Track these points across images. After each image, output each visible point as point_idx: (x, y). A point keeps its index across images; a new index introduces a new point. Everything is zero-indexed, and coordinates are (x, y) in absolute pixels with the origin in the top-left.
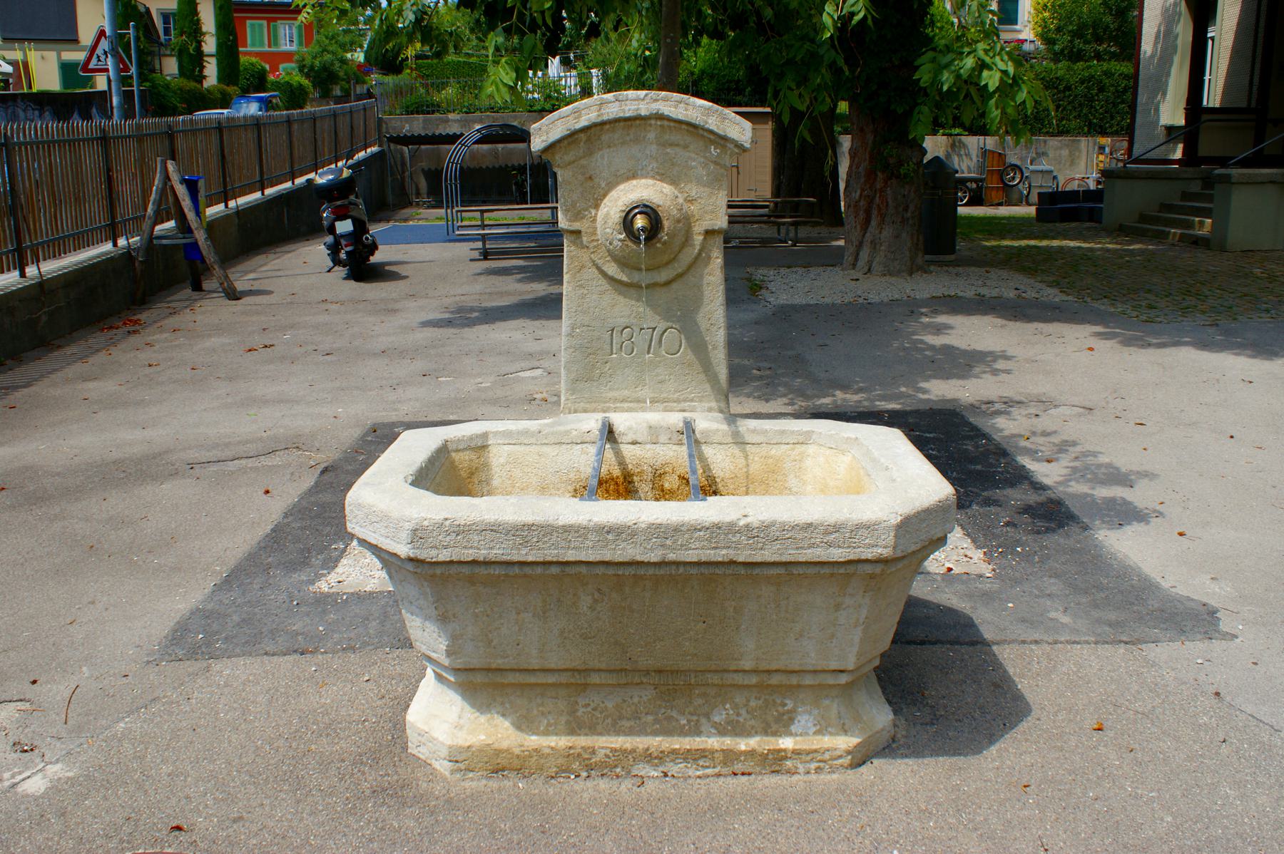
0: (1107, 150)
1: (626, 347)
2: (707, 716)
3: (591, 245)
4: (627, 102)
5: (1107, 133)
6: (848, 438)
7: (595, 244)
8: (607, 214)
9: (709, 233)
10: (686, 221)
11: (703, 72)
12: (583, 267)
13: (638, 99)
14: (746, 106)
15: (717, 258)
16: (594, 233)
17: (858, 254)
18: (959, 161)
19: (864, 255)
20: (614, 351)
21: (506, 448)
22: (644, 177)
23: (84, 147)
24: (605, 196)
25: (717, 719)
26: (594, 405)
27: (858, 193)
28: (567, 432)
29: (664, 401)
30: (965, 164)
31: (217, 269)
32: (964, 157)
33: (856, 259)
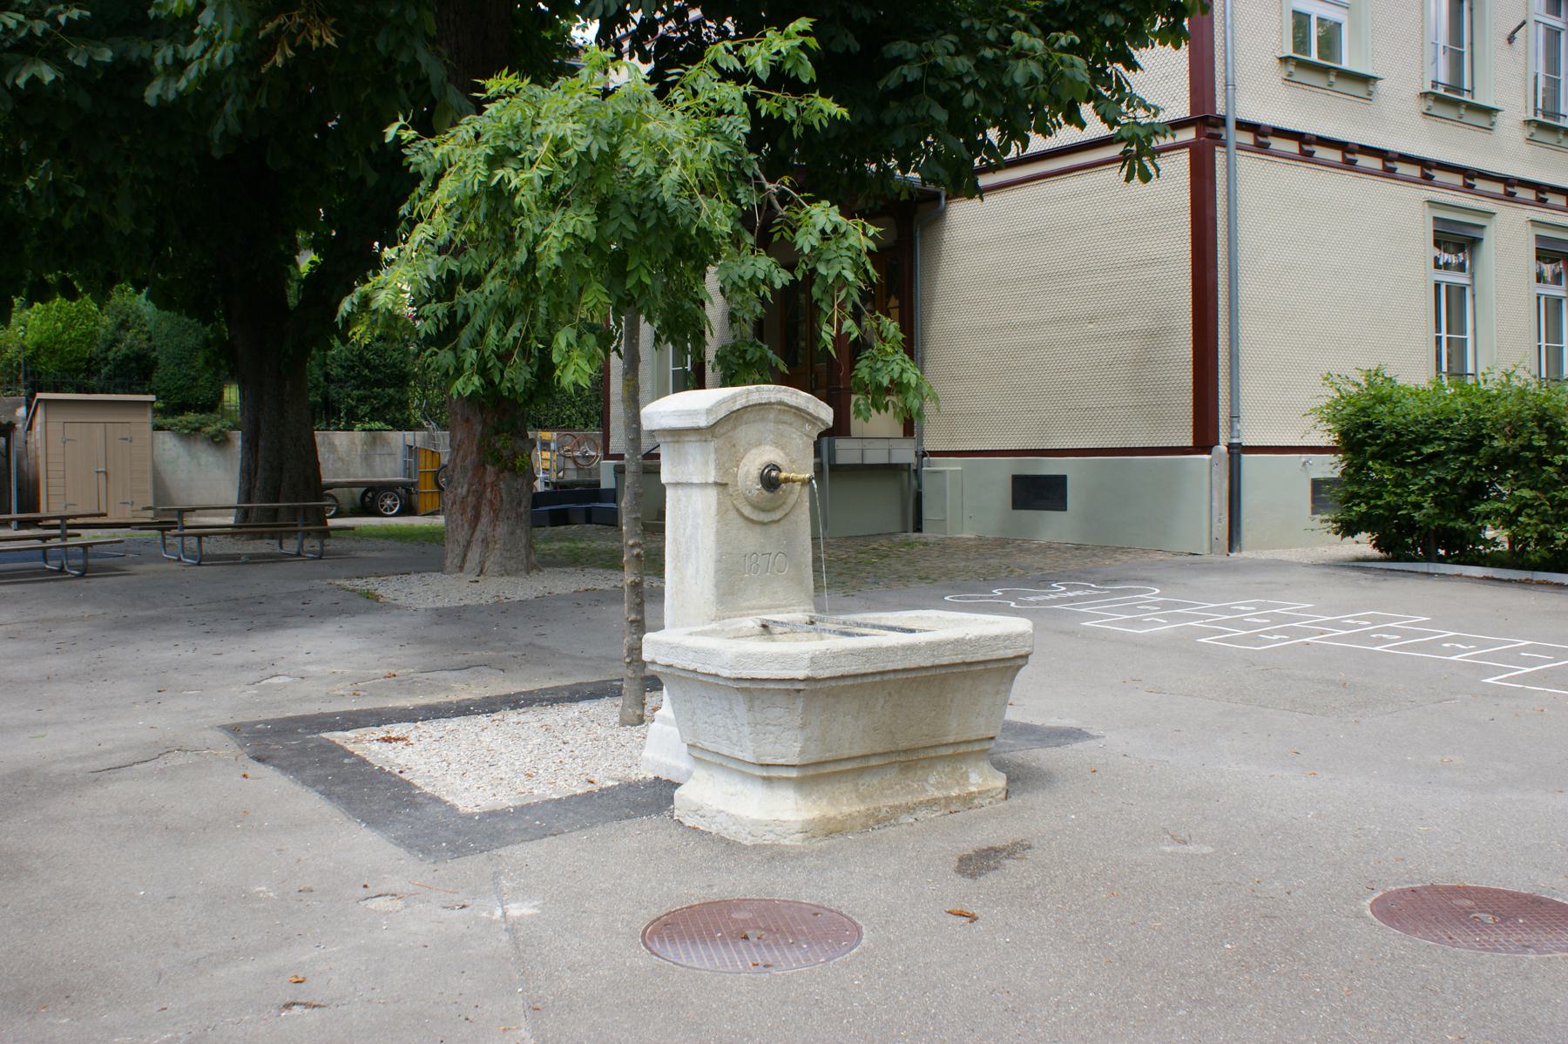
0: (553, 446)
2: (926, 781)
5: (546, 427)
11: (39, 346)
12: (727, 510)
13: (769, 390)
14: (102, 392)
16: (736, 485)
17: (465, 556)
19: (474, 555)
25: (931, 782)
26: (735, 613)
27: (466, 487)
28: (739, 630)
29: (779, 606)
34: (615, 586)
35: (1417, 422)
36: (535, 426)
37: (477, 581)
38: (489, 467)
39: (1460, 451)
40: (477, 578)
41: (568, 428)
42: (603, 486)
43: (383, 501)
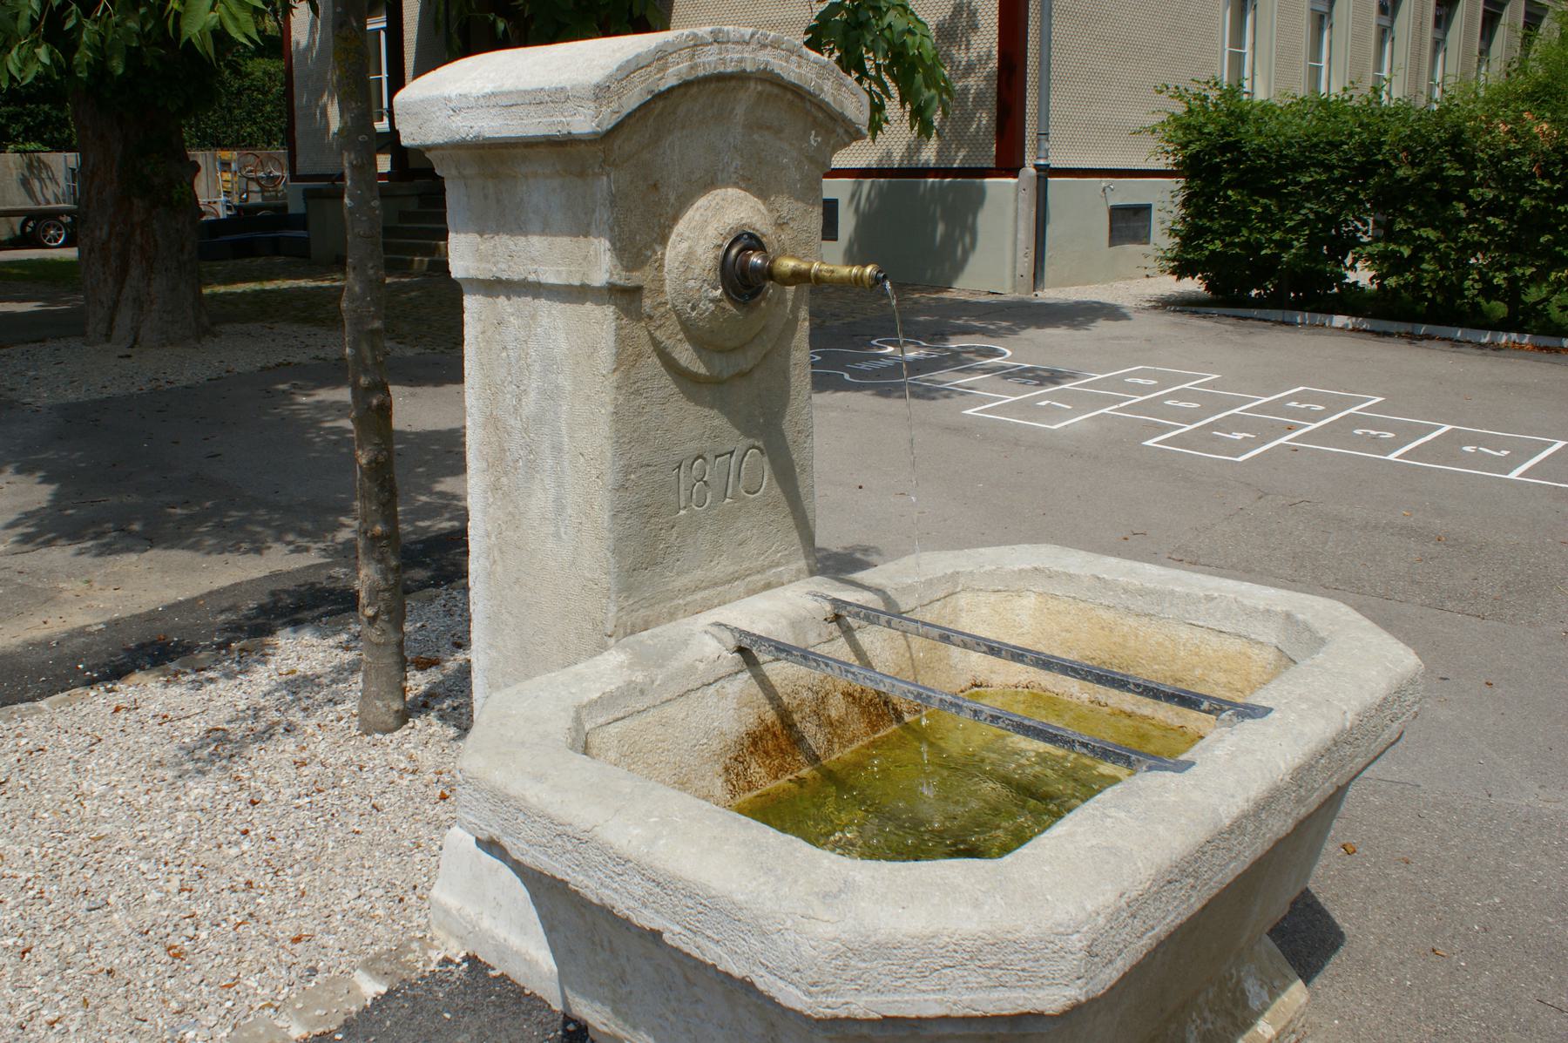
1: (698, 492)
3: (657, 313)
4: (730, 46)
5: (226, 146)
6: (1021, 571)
7: (663, 310)
8: (690, 254)
12: (640, 355)
15: (805, 320)
16: (661, 291)
17: (112, 320)
18: (42, 188)
19: (124, 319)
20: (682, 505)
21: (614, 729)
22: (726, 185)
24: (675, 219)
27: (106, 228)
28: (691, 669)
30: (51, 191)
32: (48, 181)
33: (110, 327)
34: (317, 358)
35: (1290, 145)
36: (213, 145)
37: (129, 356)
38: (136, 201)
39: (1343, 180)
40: (129, 351)
41: (251, 146)
42: (291, 210)
43: (45, 231)
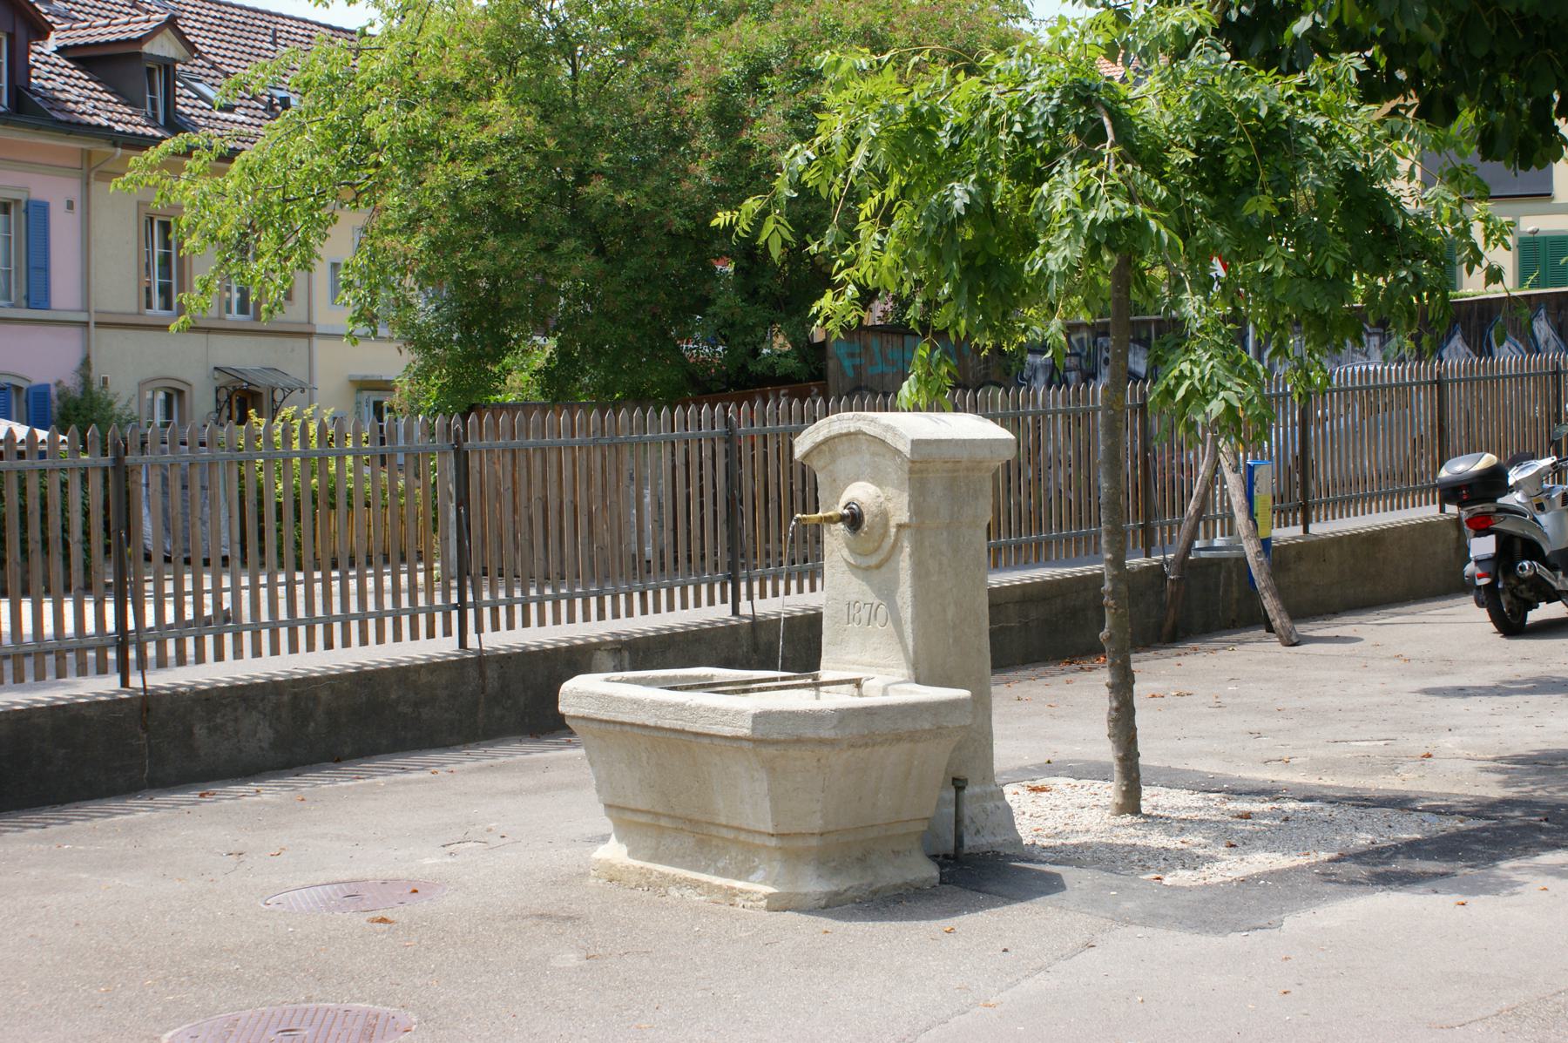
9: (900, 526)
10: (884, 516)
22: (863, 480)
23: (1418, 395)
31: (1269, 599)
